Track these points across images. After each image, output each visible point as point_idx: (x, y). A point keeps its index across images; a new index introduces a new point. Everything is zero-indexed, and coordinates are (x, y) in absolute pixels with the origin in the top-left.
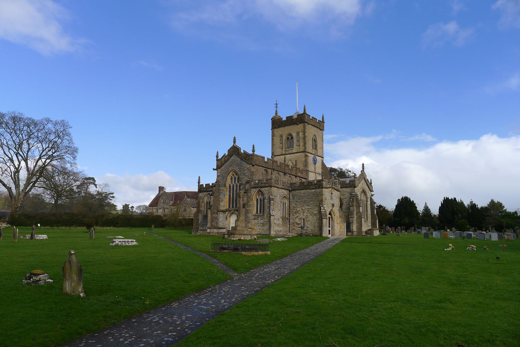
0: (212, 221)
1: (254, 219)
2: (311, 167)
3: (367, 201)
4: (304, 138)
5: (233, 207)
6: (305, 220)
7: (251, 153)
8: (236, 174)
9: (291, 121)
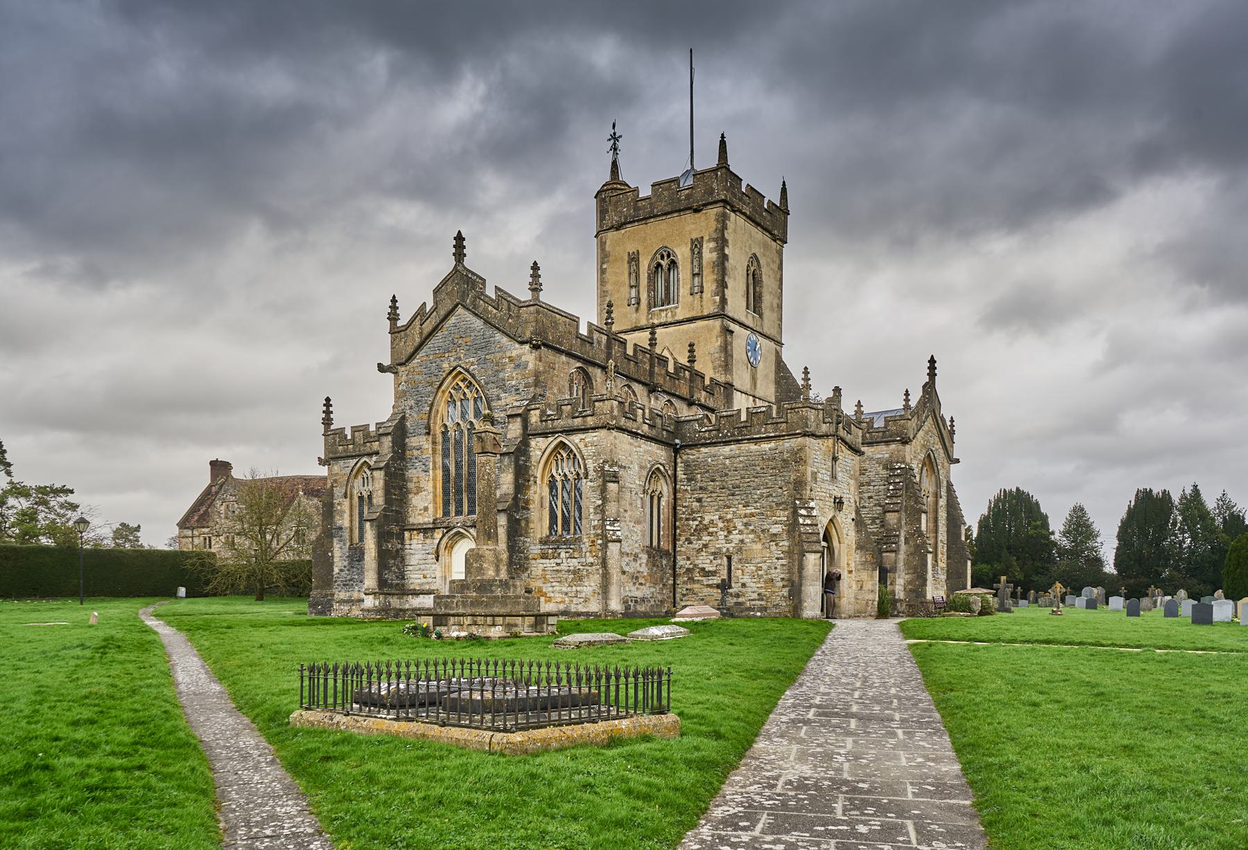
0: (382, 565)
1: (544, 556)
2: (741, 378)
3: (937, 496)
5: (459, 513)
6: (735, 558)
7: (525, 295)
8: (470, 385)
9: (674, 200)
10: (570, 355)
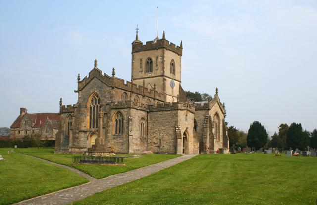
2: (169, 90)
4: (163, 63)
5: (93, 127)
7: (111, 76)
8: (97, 96)
9: (150, 46)
10: (122, 89)
